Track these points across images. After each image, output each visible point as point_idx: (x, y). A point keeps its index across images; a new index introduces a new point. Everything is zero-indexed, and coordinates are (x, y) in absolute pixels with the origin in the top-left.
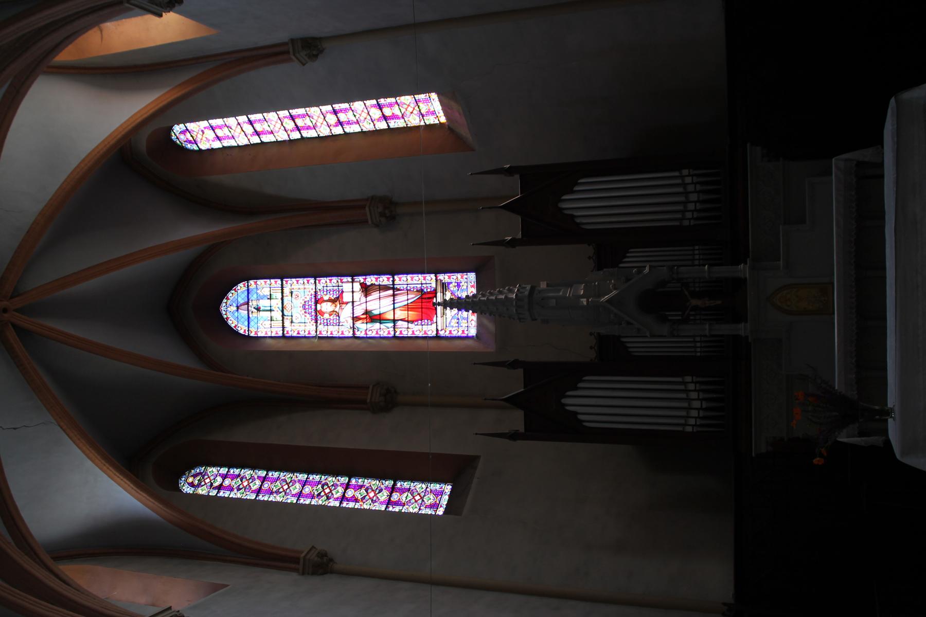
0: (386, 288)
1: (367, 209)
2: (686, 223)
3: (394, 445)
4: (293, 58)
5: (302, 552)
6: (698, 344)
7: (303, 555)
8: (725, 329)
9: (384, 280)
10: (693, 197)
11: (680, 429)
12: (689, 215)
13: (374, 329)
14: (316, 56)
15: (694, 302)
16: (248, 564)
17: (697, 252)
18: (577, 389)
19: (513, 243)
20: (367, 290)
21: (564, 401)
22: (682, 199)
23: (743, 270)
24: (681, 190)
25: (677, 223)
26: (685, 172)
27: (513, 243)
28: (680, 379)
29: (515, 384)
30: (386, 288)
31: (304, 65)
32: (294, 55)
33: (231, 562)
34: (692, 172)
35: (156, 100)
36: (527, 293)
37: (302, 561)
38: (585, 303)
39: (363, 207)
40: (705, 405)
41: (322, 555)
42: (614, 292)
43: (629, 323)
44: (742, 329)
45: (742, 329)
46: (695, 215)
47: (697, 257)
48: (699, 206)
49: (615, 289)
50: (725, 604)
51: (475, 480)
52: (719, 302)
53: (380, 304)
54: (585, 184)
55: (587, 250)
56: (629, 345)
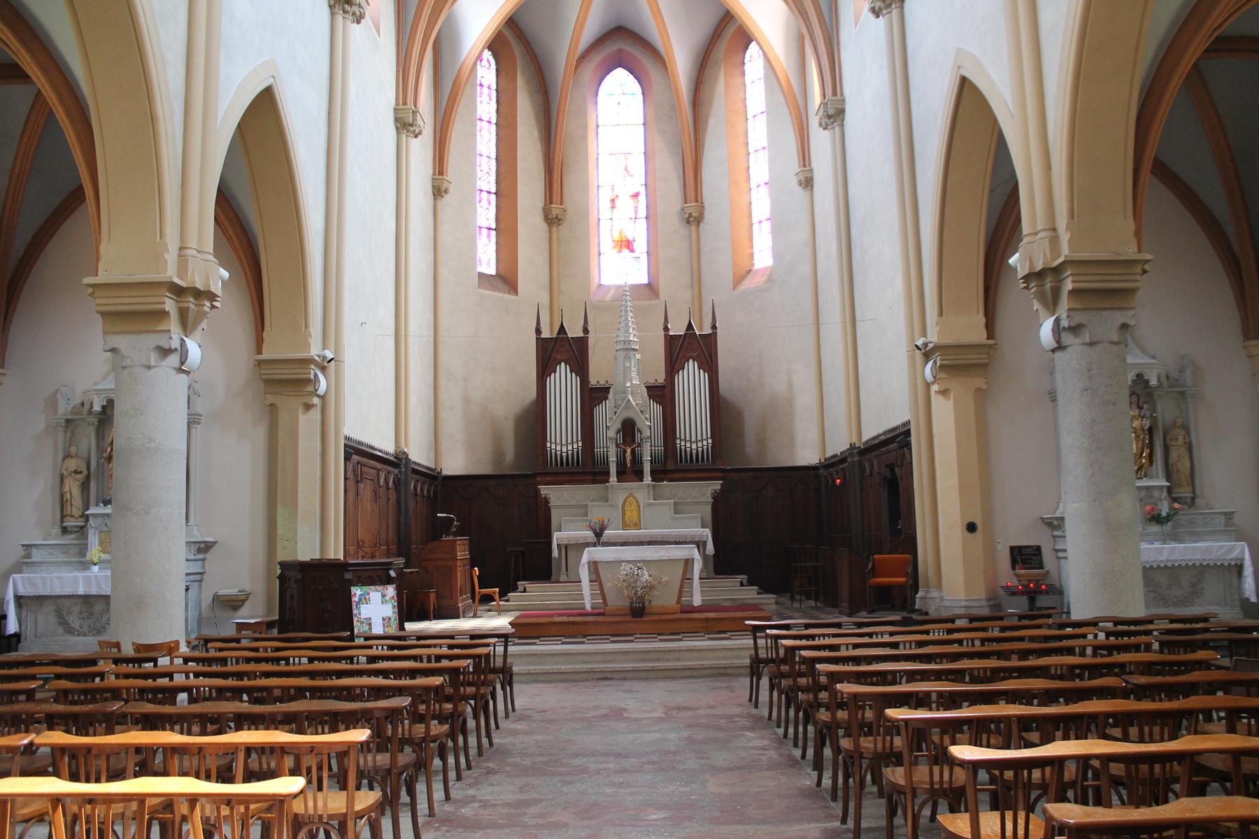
0: (636, 213)
1: (695, 204)
2: (678, 441)
3: (522, 230)
4: (800, 170)
5: (447, 176)
6: (602, 450)
7: (446, 178)
8: (613, 469)
9: (642, 212)
10: (694, 446)
11: (548, 439)
12: (683, 443)
13: (604, 204)
14: (801, 185)
15: (629, 451)
16: (435, 132)
17: (657, 448)
18: (571, 372)
19: (666, 329)
20: (636, 195)
21: (563, 364)
22: (693, 439)
23: (648, 479)
24: (699, 438)
25: (678, 436)
26: (710, 441)
27: (666, 329)
28: (579, 439)
29: (574, 331)
30: (636, 213)
31: (796, 175)
32: (802, 171)
33: (435, 118)
34: (710, 445)
35: (778, 59)
36: (633, 347)
37: (441, 177)
38: (627, 385)
39: (696, 201)
40: (564, 454)
41: (446, 192)
42: (634, 404)
43: (616, 413)
44: (613, 478)
45: (613, 478)
46: (683, 448)
47: (657, 448)
48: (688, 449)
49: (636, 404)
50: (441, 469)
51: (501, 295)
52: (629, 465)
53: (625, 205)
54: (704, 377)
55: (661, 378)
56: (600, 406)
